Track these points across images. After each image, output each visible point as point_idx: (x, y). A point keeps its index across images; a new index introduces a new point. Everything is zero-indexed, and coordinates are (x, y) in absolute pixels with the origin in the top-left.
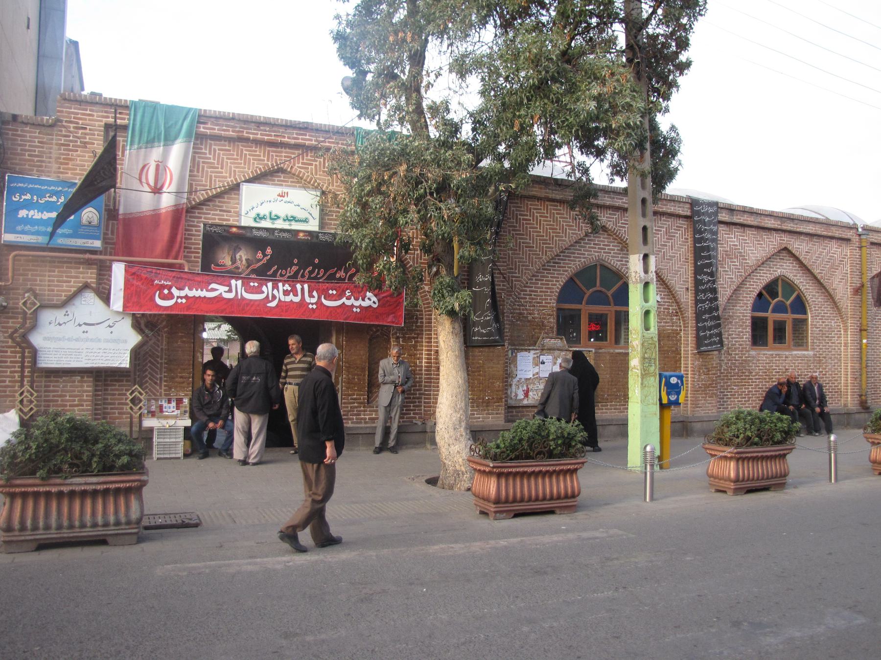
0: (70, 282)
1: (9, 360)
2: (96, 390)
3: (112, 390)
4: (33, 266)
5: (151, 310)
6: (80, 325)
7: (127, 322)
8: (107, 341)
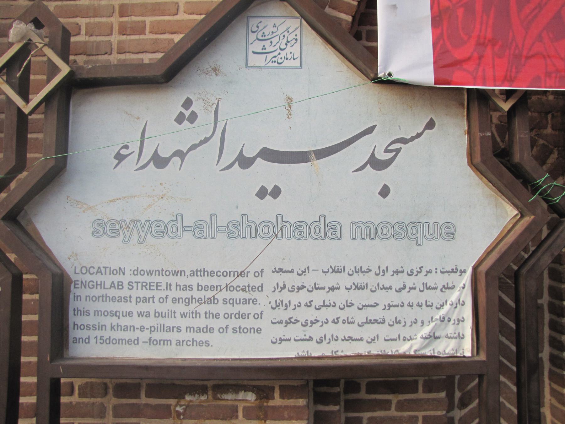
6: (244, 162)
8: (367, 231)
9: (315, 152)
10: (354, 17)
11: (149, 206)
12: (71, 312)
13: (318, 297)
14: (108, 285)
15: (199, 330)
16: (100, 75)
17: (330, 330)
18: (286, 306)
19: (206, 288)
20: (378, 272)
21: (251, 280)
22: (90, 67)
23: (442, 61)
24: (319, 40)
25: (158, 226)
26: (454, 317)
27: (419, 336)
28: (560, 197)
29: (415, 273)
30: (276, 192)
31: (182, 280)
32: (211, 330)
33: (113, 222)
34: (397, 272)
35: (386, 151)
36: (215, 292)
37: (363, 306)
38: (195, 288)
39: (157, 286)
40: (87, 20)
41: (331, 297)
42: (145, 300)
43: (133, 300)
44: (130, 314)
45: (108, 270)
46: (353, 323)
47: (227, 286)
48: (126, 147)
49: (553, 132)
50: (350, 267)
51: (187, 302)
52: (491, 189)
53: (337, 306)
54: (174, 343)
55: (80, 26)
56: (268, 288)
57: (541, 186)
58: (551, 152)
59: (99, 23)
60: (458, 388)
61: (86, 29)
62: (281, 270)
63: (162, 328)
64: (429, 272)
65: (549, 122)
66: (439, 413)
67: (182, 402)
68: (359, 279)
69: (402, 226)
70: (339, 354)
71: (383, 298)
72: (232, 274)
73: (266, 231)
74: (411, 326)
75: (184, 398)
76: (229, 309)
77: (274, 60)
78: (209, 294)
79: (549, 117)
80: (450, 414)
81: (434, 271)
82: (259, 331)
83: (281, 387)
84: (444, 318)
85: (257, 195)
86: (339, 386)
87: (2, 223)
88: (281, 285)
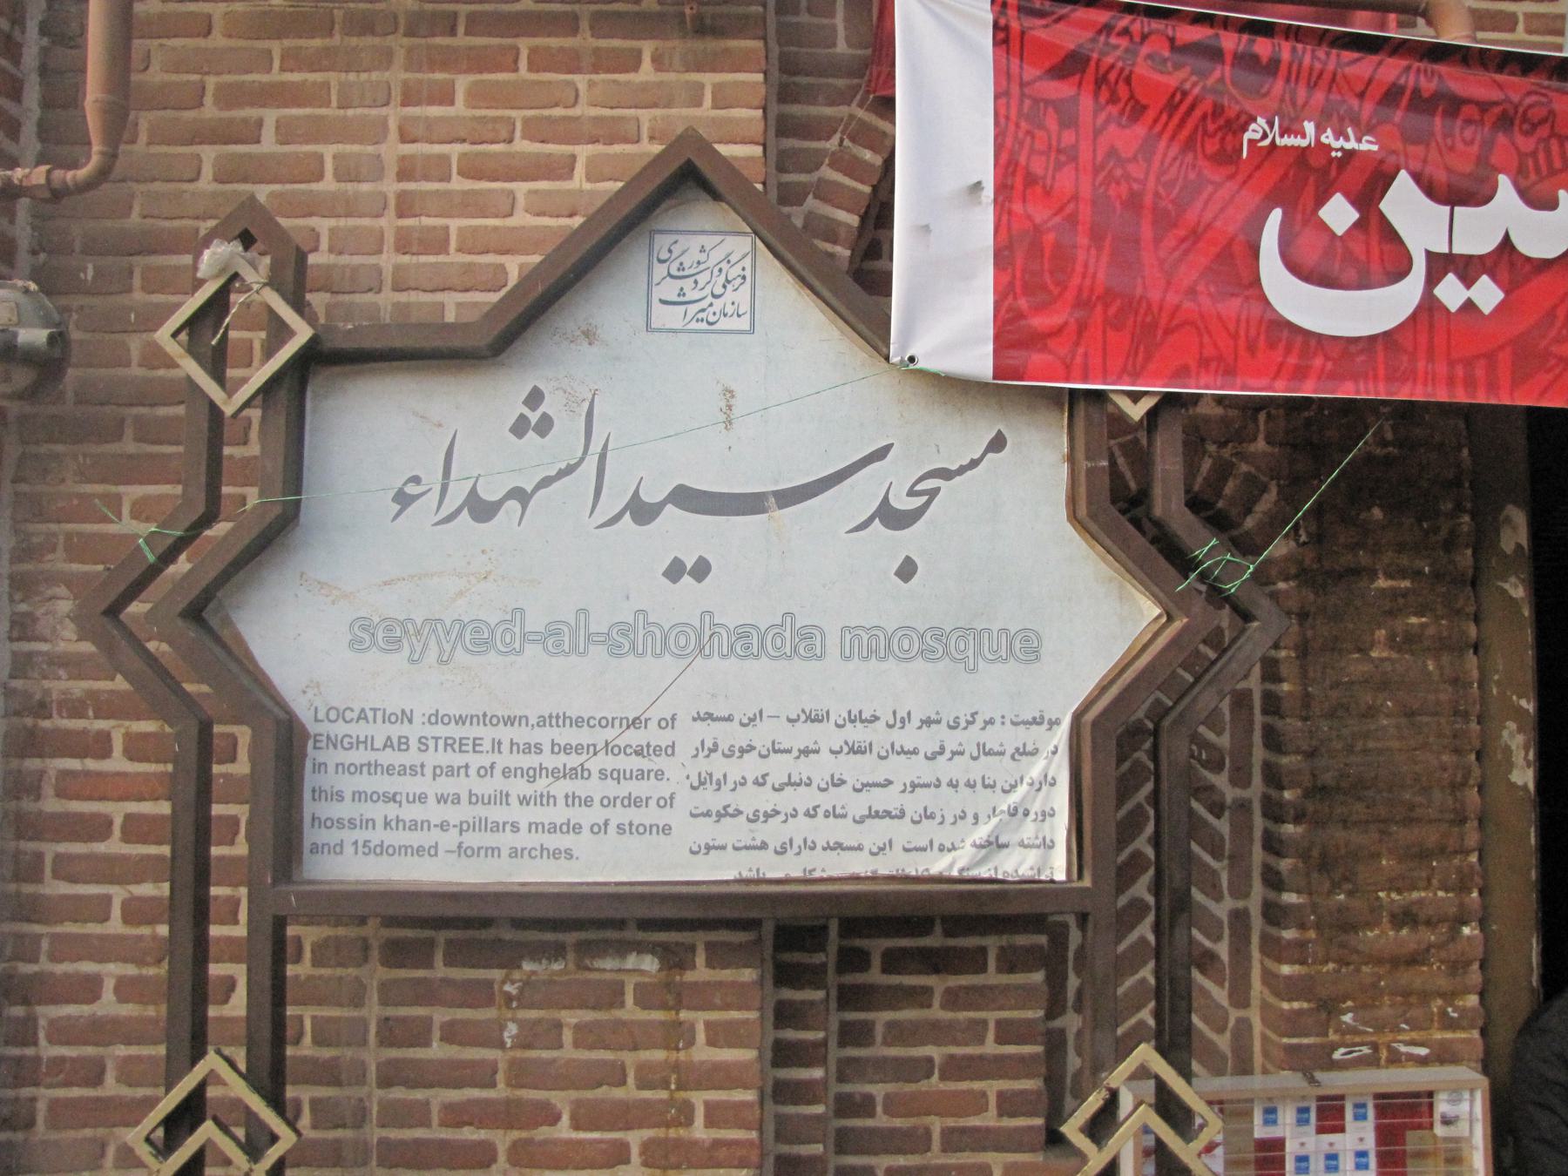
0: (564, 169)
1: (118, 811)
2: (784, 1054)
3: (898, 1034)
4: (293, 60)
5: (1229, 373)
6: (642, 511)
7: (1034, 472)
8: (873, 645)
9: (776, 494)
10: (863, 219)
11: (461, 593)
12: (307, 795)
13: (779, 768)
14: (378, 744)
15: (554, 829)
16: (368, 343)
17: (800, 828)
18: (719, 783)
19: (567, 749)
20: (891, 722)
21: (652, 735)
22: (350, 327)
23: (1011, 335)
24: (787, 278)
25: (477, 631)
26: (1036, 807)
27: (969, 842)
28: (1238, 582)
29: (963, 724)
30: (701, 570)
31: (521, 734)
32: (577, 829)
33: (389, 623)
34: (927, 722)
35: (912, 493)
36: (584, 757)
37: (864, 785)
38: (547, 748)
39: (475, 745)
40: (332, 222)
41: (804, 768)
42: (451, 771)
43: (428, 771)
44: (422, 798)
45: (379, 714)
46: (844, 816)
47: (607, 744)
48: (416, 480)
49: (1268, 449)
50: (838, 712)
51: (532, 775)
52: (1111, 566)
53: (815, 785)
54: (505, 853)
55: (318, 236)
56: (685, 750)
57: (1201, 563)
58: (1265, 489)
59: (356, 228)
60: (1075, 968)
61: (330, 239)
62: (710, 717)
63: (482, 825)
64: (991, 722)
65: (1262, 427)
66: (1030, 1014)
67: (516, 975)
68: (857, 734)
69: (939, 634)
70: (817, 875)
71: (903, 770)
72: (617, 723)
73: (682, 643)
74: (954, 823)
75: (519, 967)
76: (612, 789)
77: (700, 316)
78: (573, 761)
79: (1262, 416)
80: (1057, 1023)
81: (998, 720)
82: (666, 830)
83: (710, 947)
84: (1016, 809)
85: (666, 574)
86: (823, 950)
87: (180, 622)
88: (709, 744)
